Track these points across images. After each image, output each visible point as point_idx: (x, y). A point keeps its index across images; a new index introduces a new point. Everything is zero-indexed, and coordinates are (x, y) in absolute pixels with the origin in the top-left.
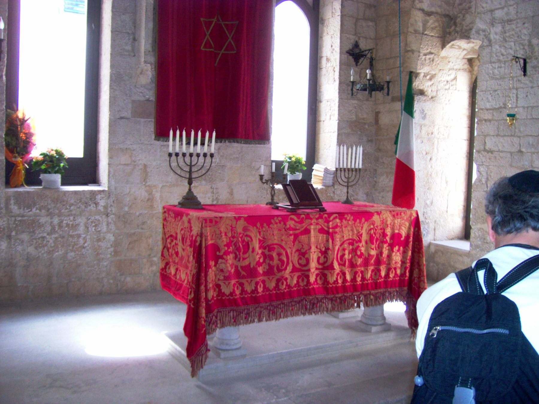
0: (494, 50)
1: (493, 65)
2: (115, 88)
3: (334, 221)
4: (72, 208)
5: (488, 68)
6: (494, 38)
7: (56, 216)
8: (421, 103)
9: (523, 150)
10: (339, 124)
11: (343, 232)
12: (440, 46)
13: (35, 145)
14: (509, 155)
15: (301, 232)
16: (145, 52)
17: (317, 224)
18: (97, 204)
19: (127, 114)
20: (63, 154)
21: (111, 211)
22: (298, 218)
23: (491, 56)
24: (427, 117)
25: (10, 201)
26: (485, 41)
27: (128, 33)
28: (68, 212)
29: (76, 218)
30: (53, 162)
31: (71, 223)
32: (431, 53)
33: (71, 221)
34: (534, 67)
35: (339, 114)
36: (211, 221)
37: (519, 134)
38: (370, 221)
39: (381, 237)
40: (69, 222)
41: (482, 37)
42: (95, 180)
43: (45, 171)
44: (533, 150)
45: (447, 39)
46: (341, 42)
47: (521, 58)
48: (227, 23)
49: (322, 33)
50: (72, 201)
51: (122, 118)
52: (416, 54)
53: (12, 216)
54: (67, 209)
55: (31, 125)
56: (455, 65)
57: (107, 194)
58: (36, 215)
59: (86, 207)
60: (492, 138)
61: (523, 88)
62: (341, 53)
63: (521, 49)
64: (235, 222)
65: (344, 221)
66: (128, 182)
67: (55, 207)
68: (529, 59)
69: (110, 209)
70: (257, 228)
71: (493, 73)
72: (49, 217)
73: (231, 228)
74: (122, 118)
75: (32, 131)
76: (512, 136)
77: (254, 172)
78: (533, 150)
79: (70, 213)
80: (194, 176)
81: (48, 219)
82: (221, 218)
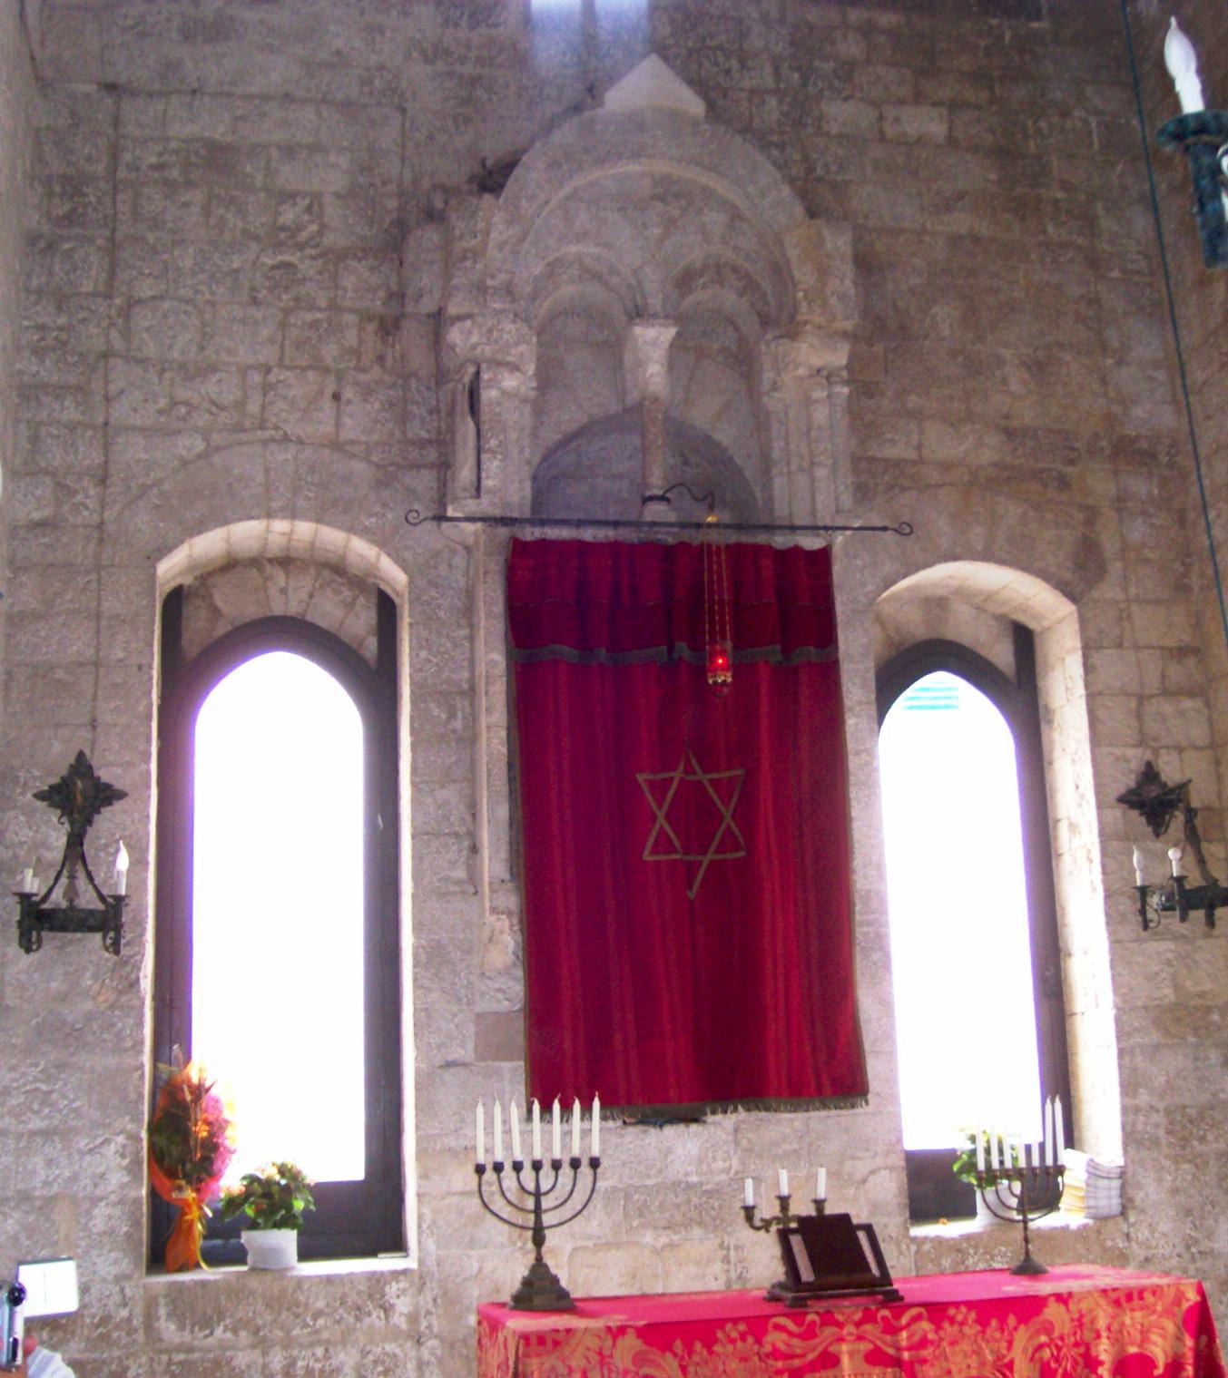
2: (427, 984)
3: (915, 1327)
4: (321, 1322)
7: (277, 1348)
11: (946, 1359)
15: (812, 1362)
16: (490, 883)
17: (860, 1338)
18: (387, 1309)
19: (465, 1052)
20: (299, 1173)
21: (429, 1327)
22: (799, 1323)
25: (156, 1311)
27: (457, 835)
28: (310, 1334)
29: (332, 1351)
30: (271, 1199)
31: (318, 1366)
33: (317, 1360)
35: (1115, 991)
36: (541, 1339)
38: (1036, 1323)
39: (1079, 1369)
40: (312, 1363)
42: (396, 1244)
43: (253, 1225)
46: (1096, 774)
48: (715, 776)
49: (1051, 752)
50: (320, 1304)
51: (449, 1064)
53: (161, 1352)
54: (306, 1325)
55: (224, 1100)
57: (419, 1280)
58: (224, 1347)
59: (357, 1318)
62: (1100, 806)
64: (609, 1343)
65: (946, 1325)
66: (472, 1243)
67: (274, 1321)
69: (424, 1324)
70: (675, 1355)
72: (257, 1352)
73: (597, 1358)
74: (449, 1064)
75: (226, 1114)
79: (313, 1338)
80: (547, 1219)
81: (256, 1355)
82: (568, 1331)
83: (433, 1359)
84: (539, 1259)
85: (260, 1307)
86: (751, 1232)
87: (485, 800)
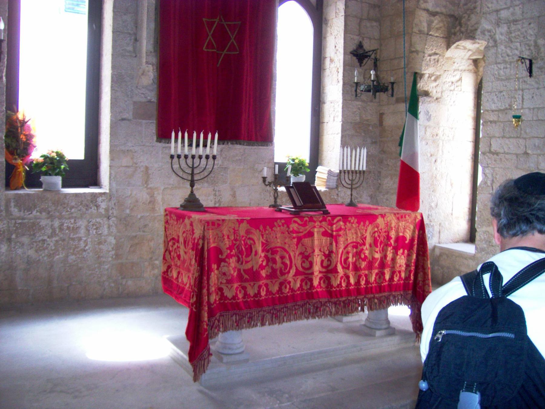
0: (499, 50)
1: (499, 66)
2: (116, 89)
3: (338, 224)
4: (73, 210)
5: (493, 69)
6: (500, 39)
8: (426, 105)
9: (529, 152)
11: (347, 235)
12: (445, 47)
13: (35, 147)
14: (514, 157)
17: (321, 227)
18: (98, 207)
19: (129, 115)
20: (63, 155)
22: (302, 221)
23: (497, 57)
24: (432, 118)
26: (491, 41)
27: (130, 34)
28: (69, 214)
29: (77, 221)
30: (53, 164)
31: (72, 226)
32: (436, 54)
33: (72, 224)
34: (540, 68)
35: (343, 116)
36: (213, 224)
37: (525, 136)
38: (374, 224)
39: (385, 240)
40: (69, 225)
41: (487, 37)
42: (96, 183)
43: (46, 173)
44: (539, 152)
45: (452, 39)
46: (345, 43)
47: (527, 59)
49: (326, 34)
50: (73, 204)
51: (123, 119)
52: (421, 54)
53: (12, 219)
54: (68, 211)
56: (460, 66)
57: (109, 196)
58: (36, 218)
59: (87, 209)
60: (498, 139)
61: (529, 89)
62: (345, 53)
63: (526, 50)
64: (237, 225)
65: (348, 223)
67: (56, 209)
68: (535, 60)
69: (111, 212)
70: (260, 231)
71: (499, 74)
73: (233, 231)
74: (123, 119)
75: (32, 132)
76: (517, 137)
78: (539, 152)
80: (196, 178)
81: (48, 222)
82: (223, 220)
83: (113, 225)
84: (192, 192)
85: (50, 204)
86: (263, 184)
87: (146, 20)
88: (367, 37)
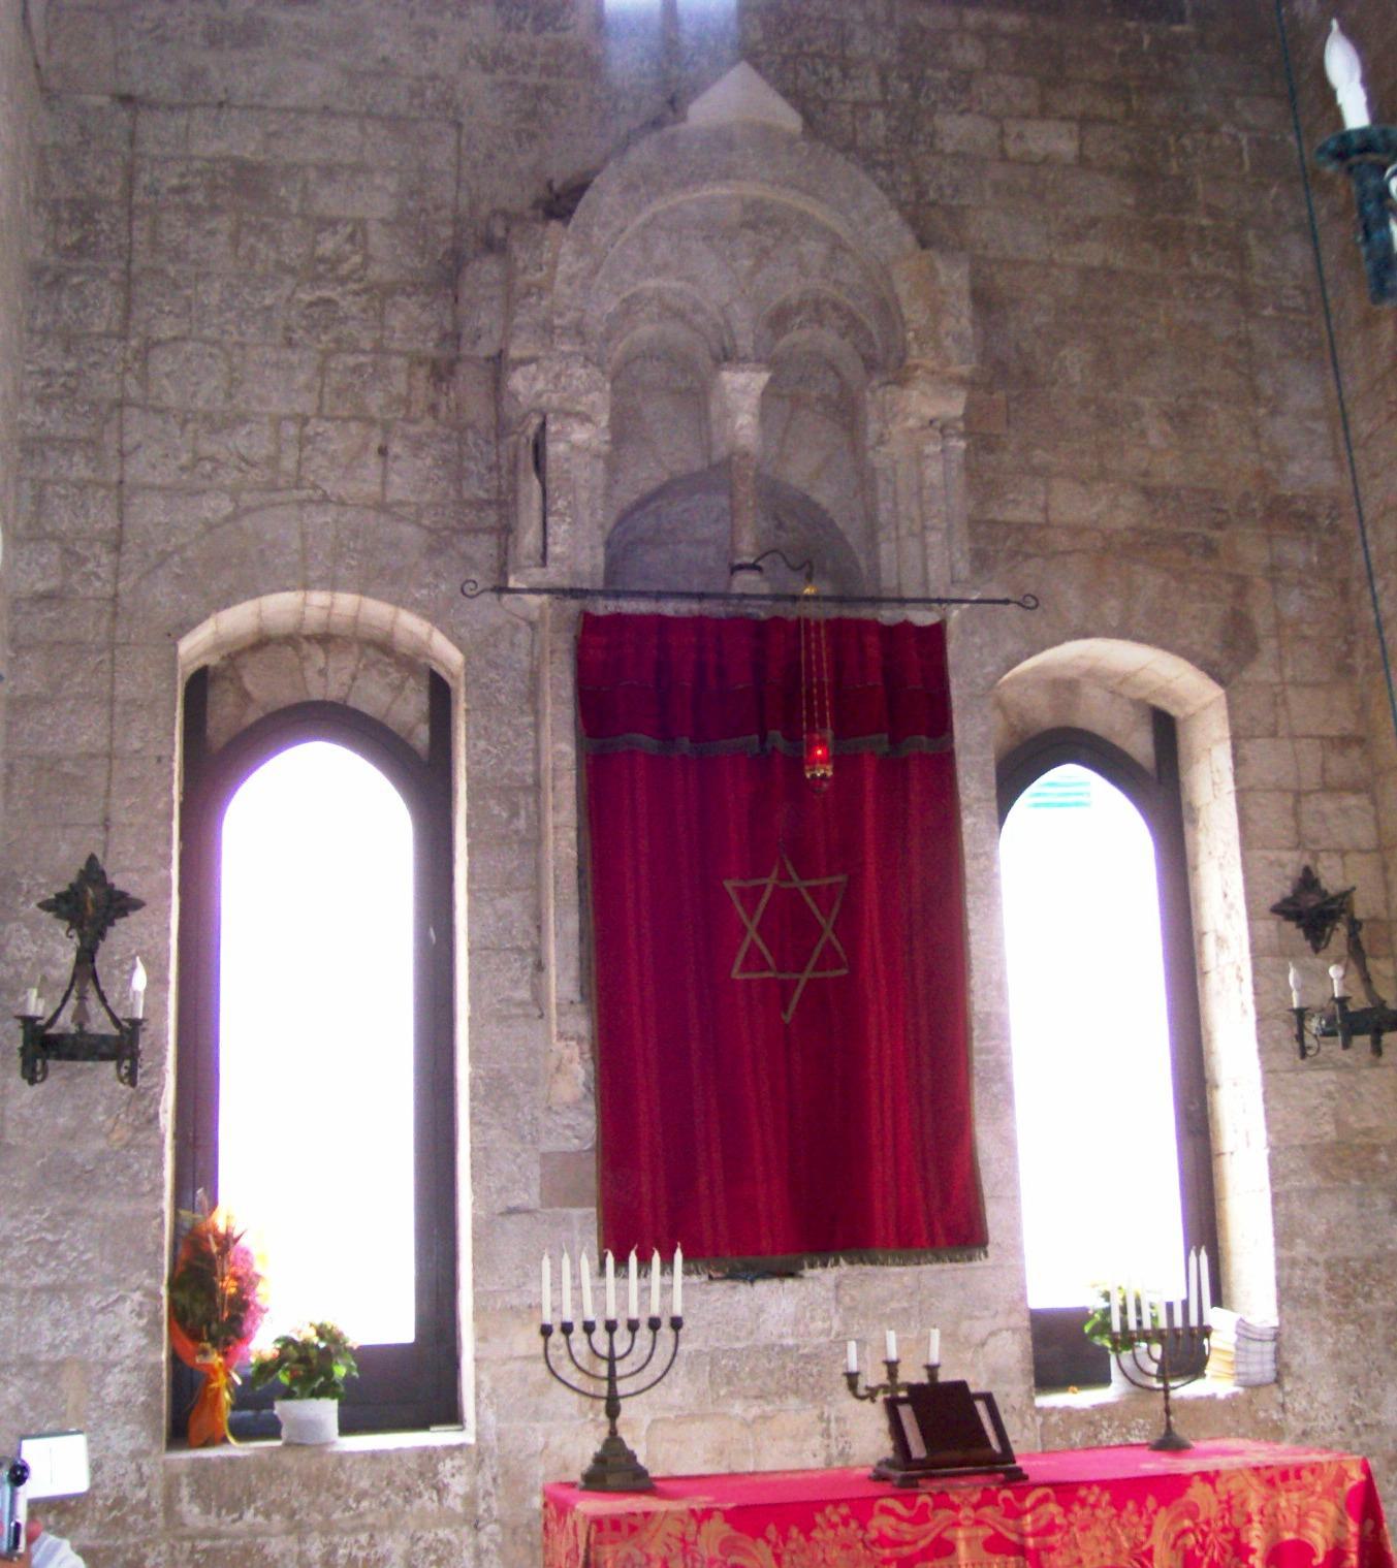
2: (486, 1119)
3: (1041, 1509)
4: (365, 1504)
7: (316, 1534)
10: (1272, 1160)
11: (1076, 1546)
13: (264, 1311)
16: (558, 1005)
17: (978, 1523)
18: (441, 1490)
19: (529, 1197)
20: (340, 1334)
21: (488, 1510)
22: (909, 1505)
27: (519, 950)
28: (352, 1518)
29: (377, 1537)
30: (308, 1365)
31: (362, 1554)
33: (361, 1548)
35: (1269, 1128)
36: (616, 1524)
38: (1178, 1505)
39: (1228, 1558)
40: (355, 1551)
42: (451, 1415)
43: (288, 1394)
46: (1247, 881)
48: (813, 883)
49: (1196, 855)
50: (365, 1484)
51: (511, 1211)
53: (183, 1538)
54: (348, 1508)
55: (255, 1252)
57: (477, 1457)
58: (254, 1532)
59: (407, 1500)
62: (1252, 917)
64: (692, 1528)
65: (1076, 1508)
66: (537, 1415)
67: (312, 1503)
69: (482, 1506)
70: (768, 1542)
72: (293, 1538)
74: (511, 1211)
77: (969, 1355)
79: (356, 1522)
80: (623, 1387)
81: (291, 1542)
82: (647, 1514)
83: (492, 1547)
84: (613, 1432)
85: (296, 1487)
87: (552, 911)
88: (1327, 850)
